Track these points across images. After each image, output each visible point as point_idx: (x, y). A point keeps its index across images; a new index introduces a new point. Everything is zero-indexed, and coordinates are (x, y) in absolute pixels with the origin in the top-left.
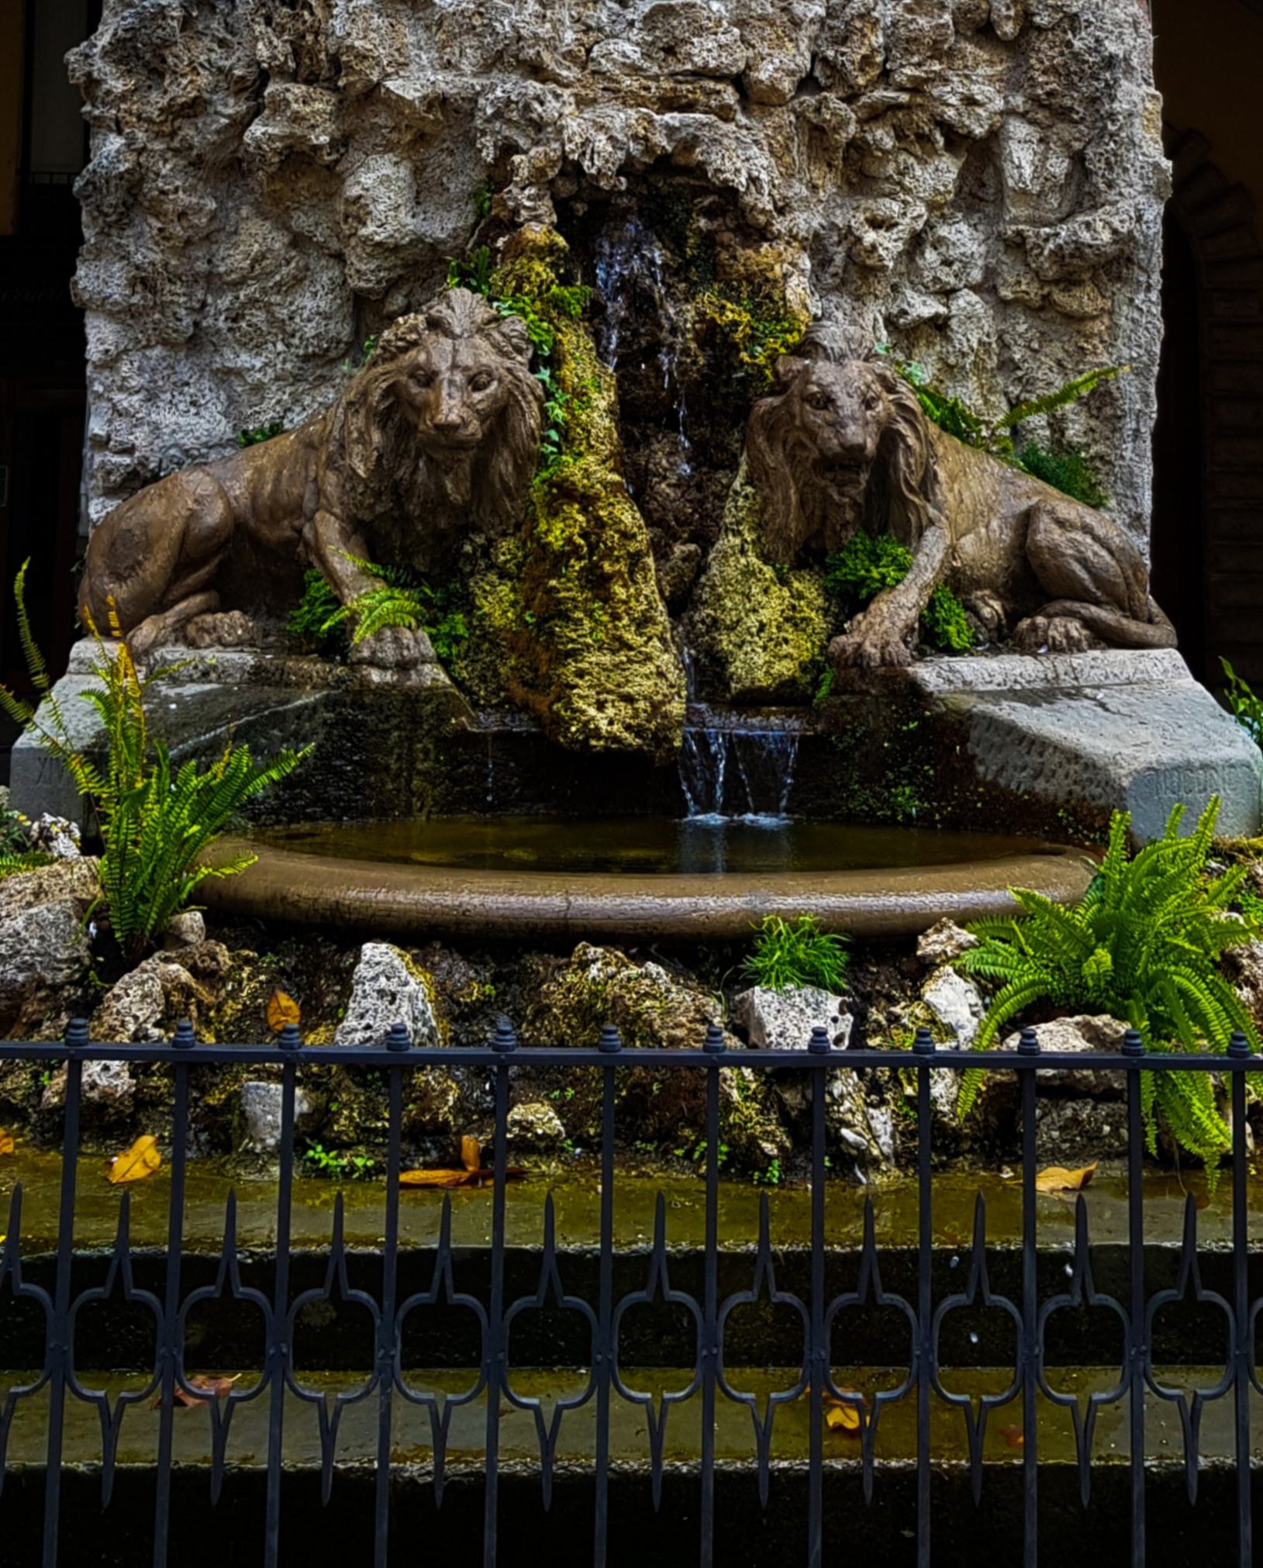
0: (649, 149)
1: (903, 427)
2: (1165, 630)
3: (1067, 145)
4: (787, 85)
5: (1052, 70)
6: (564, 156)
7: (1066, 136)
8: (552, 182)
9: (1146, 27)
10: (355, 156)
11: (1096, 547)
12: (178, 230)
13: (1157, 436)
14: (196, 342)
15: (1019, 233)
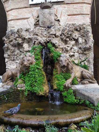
0: (47, 41)
1: (69, 63)
2: (96, 81)
3: (84, 39)
4: (59, 35)
5: (83, 32)
6: (39, 42)
7: (84, 38)
8: (38, 44)
9: (91, 29)
10: (24, 44)
11: (89, 74)
12: (11, 51)
13: (94, 64)
14: (14, 60)
15: (80, 47)
